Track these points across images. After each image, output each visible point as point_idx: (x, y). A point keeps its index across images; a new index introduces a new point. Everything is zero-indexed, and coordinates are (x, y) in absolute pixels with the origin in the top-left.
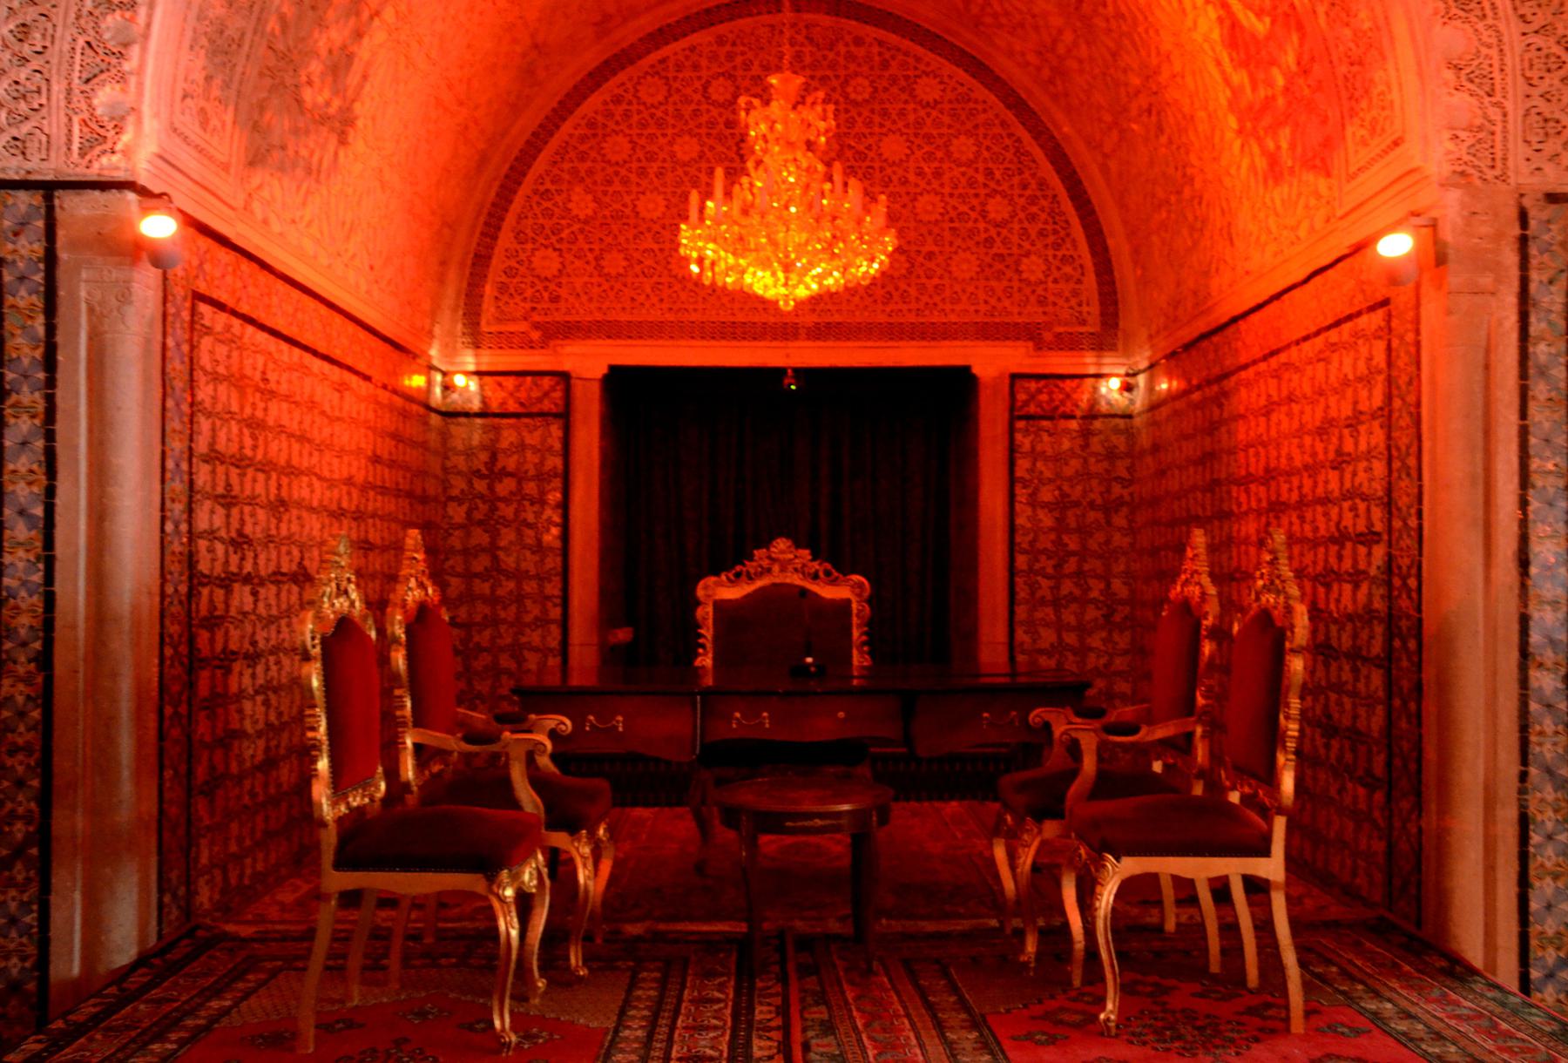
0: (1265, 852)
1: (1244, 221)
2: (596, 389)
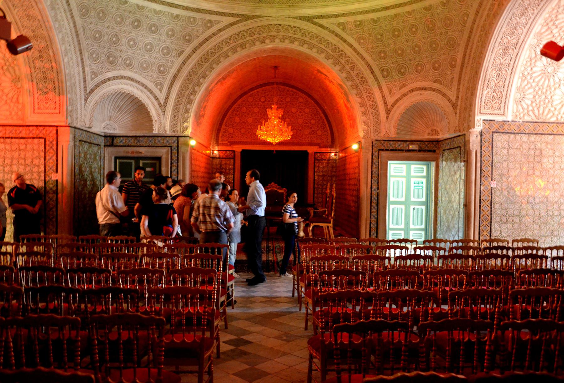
0: (330, 223)
1: (348, 132)
2: (239, 154)
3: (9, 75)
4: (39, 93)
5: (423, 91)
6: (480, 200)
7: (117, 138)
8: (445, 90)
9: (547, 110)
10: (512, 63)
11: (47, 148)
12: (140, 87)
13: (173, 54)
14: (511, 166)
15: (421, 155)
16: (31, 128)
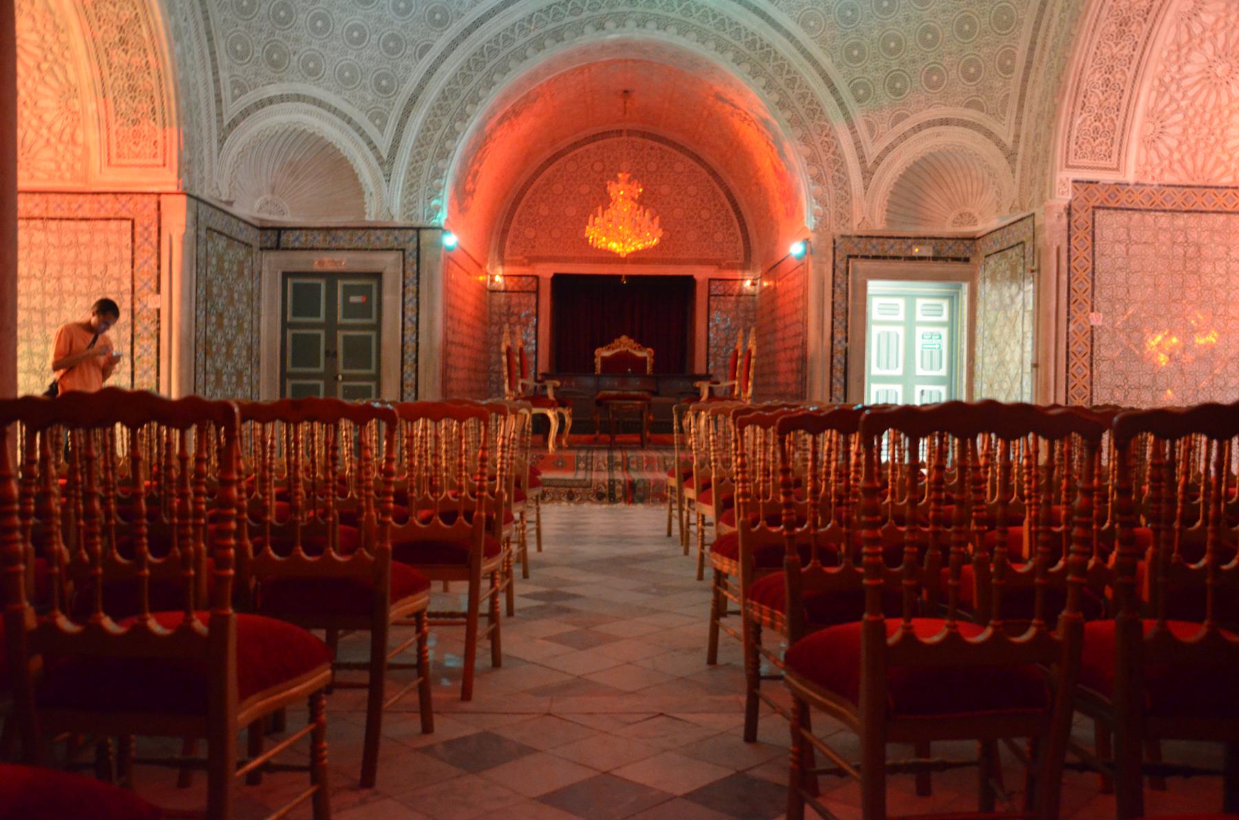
2: (549, 283)
3: (54, 84)
4: (120, 122)
5: (943, 128)
6: (1068, 353)
7: (288, 232)
8: (989, 123)
9: (1213, 159)
10: (1137, 54)
11: (138, 240)
12: (338, 120)
13: (408, 52)
14: (1134, 280)
15: (938, 267)
16: (103, 198)
